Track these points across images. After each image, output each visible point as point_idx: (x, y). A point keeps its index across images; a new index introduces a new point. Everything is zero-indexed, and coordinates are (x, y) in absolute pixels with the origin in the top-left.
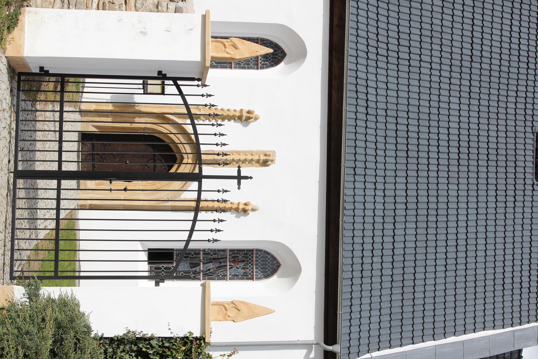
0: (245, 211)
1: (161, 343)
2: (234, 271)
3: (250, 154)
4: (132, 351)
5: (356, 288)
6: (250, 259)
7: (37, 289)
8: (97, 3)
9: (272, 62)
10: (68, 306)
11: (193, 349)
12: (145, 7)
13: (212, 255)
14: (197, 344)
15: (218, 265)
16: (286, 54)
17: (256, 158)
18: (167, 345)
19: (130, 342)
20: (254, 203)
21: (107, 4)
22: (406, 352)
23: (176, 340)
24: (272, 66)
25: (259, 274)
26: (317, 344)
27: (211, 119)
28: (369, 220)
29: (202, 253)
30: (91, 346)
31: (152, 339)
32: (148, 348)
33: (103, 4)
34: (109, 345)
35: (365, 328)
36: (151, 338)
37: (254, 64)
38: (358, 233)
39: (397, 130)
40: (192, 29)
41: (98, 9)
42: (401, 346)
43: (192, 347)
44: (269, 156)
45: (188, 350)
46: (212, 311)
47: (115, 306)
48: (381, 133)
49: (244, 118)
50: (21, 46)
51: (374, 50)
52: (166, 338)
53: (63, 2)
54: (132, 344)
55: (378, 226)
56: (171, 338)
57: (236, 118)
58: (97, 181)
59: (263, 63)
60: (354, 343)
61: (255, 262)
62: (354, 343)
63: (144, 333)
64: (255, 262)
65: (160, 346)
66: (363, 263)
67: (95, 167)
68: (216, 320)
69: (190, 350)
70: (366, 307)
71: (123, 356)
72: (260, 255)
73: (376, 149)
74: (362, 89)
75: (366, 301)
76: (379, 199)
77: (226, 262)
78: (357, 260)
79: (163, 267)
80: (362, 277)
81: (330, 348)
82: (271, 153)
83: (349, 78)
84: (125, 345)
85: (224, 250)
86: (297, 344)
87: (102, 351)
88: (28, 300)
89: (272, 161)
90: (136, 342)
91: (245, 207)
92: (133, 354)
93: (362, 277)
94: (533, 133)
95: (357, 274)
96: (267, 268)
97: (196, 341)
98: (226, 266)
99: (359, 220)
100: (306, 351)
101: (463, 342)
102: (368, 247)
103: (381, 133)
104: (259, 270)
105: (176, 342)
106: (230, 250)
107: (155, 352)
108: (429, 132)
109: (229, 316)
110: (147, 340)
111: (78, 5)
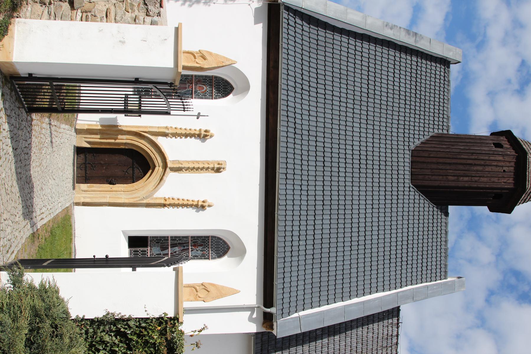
0: (203, 207)
2: (195, 253)
4: (111, 331)
5: (288, 264)
7: (21, 275)
10: (47, 293)
14: (171, 324)
15: (182, 248)
16: (234, 89)
17: (211, 166)
18: (144, 325)
20: (210, 201)
21: (90, 17)
22: (324, 311)
23: (152, 320)
24: (223, 97)
26: (258, 307)
28: (296, 213)
31: (130, 320)
32: (126, 329)
34: (90, 326)
35: (294, 294)
36: (129, 319)
38: (289, 223)
39: (316, 146)
40: (166, 39)
41: (82, 20)
42: (319, 306)
43: (166, 327)
44: (221, 164)
45: (163, 330)
46: (184, 293)
48: (305, 148)
49: (202, 136)
50: (10, 52)
51: (300, 86)
52: (142, 319)
53: (50, 15)
54: (111, 324)
55: (303, 218)
56: (148, 319)
58: (89, 185)
60: (286, 305)
61: (212, 246)
62: (286, 305)
63: (122, 314)
64: (212, 246)
65: (137, 327)
66: (292, 246)
70: (294, 279)
71: (102, 336)
73: (302, 160)
74: (291, 114)
75: (294, 274)
76: (304, 198)
77: (188, 246)
78: (288, 244)
80: (292, 256)
81: (268, 310)
82: (222, 163)
83: (282, 106)
84: (105, 325)
85: (187, 237)
86: (243, 308)
87: (83, 331)
88: (12, 286)
89: (224, 169)
90: (115, 323)
91: (203, 203)
93: (292, 256)
94: (409, 150)
95: (288, 254)
96: (219, 250)
97: (170, 321)
98: (188, 249)
99: (289, 213)
100: (250, 312)
101: (363, 302)
102: (296, 233)
103: (305, 148)
105: (151, 322)
106: (192, 237)
107: (132, 332)
108: (339, 148)
110: (125, 321)
111: (63, 18)
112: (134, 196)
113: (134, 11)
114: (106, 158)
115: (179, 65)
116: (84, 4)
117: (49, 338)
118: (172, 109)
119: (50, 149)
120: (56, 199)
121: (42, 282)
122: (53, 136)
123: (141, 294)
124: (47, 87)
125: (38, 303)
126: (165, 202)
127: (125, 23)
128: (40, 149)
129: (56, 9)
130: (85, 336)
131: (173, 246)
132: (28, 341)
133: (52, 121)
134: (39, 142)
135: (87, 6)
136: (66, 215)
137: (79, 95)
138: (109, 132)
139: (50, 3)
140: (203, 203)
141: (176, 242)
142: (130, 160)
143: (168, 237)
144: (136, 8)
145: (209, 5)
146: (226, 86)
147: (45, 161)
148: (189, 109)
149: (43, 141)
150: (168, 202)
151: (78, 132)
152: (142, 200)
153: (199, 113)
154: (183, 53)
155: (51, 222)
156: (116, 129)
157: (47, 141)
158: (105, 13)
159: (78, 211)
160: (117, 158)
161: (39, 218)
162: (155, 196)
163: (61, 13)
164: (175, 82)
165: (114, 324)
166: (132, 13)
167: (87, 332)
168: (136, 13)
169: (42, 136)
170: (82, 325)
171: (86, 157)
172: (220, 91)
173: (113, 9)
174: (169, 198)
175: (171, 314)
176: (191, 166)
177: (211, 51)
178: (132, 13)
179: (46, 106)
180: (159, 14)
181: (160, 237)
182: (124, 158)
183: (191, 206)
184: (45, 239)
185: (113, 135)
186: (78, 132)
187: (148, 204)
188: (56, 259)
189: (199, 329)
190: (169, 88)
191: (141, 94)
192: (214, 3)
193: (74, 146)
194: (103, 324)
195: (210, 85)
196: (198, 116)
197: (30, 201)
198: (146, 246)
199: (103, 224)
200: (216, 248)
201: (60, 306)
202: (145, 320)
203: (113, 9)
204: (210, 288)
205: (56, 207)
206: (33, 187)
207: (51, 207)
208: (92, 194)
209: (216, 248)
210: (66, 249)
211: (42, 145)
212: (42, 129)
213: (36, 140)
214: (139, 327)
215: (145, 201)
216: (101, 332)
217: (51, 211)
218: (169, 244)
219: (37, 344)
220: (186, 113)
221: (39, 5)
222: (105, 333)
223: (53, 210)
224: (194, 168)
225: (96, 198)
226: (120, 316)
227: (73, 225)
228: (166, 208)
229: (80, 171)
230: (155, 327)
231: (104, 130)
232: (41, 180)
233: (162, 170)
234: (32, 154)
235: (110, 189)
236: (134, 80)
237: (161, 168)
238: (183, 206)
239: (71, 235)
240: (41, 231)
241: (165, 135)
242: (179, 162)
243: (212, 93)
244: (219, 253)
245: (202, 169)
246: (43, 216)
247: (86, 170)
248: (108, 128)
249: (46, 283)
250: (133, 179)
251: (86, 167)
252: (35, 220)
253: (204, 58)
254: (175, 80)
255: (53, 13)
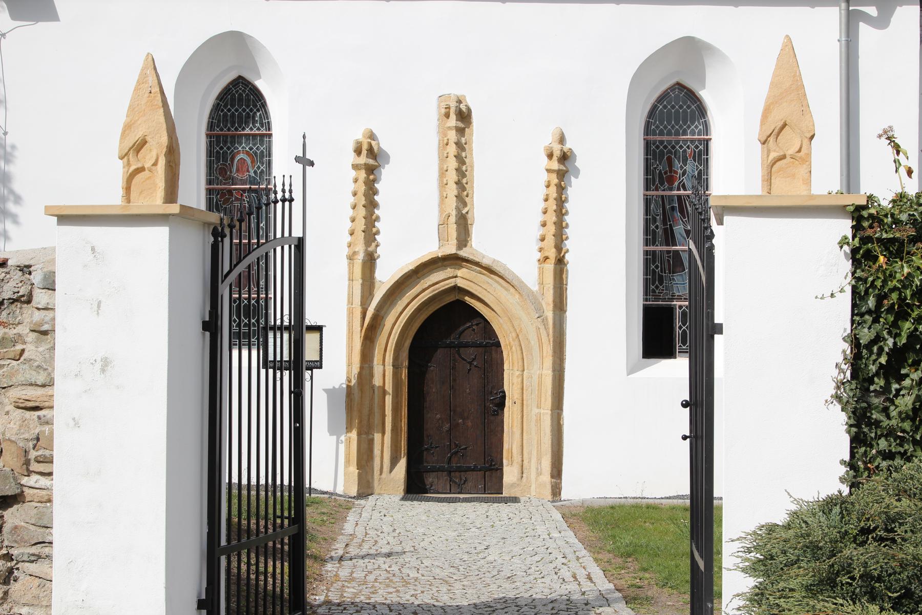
0: (565, 158)
1: (867, 317)
3: (444, 149)
4: (886, 389)
6: (665, 147)
8: (38, 477)
9: (255, 106)
10: (773, 554)
11: (885, 236)
12: (45, 362)
13: (657, 227)
14: (871, 227)
17: (452, 136)
18: (871, 302)
19: (863, 396)
20: (548, 139)
21: (40, 453)
23: (858, 279)
24: (264, 105)
25: (696, 127)
27: (374, 230)
29: (652, 248)
30: (879, 497)
31: (857, 340)
32: (881, 350)
33: (39, 462)
34: (871, 447)
36: (854, 341)
37: (262, 144)
40: (93, 249)
41: (50, 474)
43: (880, 240)
44: (448, 108)
45: (887, 249)
46: (787, 190)
47: (788, 450)
49: (371, 162)
52: (854, 306)
53: (39, 557)
54: (868, 390)
57: (372, 177)
59: (258, 125)
63: (840, 359)
65: (876, 321)
67: (475, 466)
68: (808, 182)
69: (886, 244)
71: (900, 413)
72: (657, 127)
77: (671, 198)
79: (680, 328)
82: (443, 105)
84: (870, 407)
85: (647, 202)
87: (884, 464)
90: (864, 380)
91: (555, 158)
92: (895, 386)
96: (685, 112)
97: (864, 229)
98: (679, 197)
100: (861, 25)
104: (689, 127)
105: (865, 281)
106: (647, 188)
107: (890, 333)
109: (799, 151)
111: (45, 523)
112: (534, 342)
113: (20, 335)
114: (434, 417)
115: (161, 211)
116: (8, 469)
117: (894, 550)
118: (286, 234)
119: (407, 558)
120: (539, 542)
121: (744, 570)
122: (372, 552)
123: (786, 303)
124: (234, 564)
125: (798, 578)
126: (552, 260)
127: (52, 358)
128: (406, 583)
129: (22, 542)
130: (898, 461)
131: (670, 238)
132: (902, 605)
133: (333, 554)
134: (388, 586)
135: (10, 460)
136: (584, 519)
137: (270, 489)
138: (366, 411)
139: (8, 557)
140: (555, 158)
141: (660, 231)
142: (440, 354)
143: (646, 253)
144: (12, 332)
145: (13, 147)
146: (233, 99)
147: (438, 571)
148: (287, 188)
149: (384, 575)
150: (552, 253)
151: (365, 490)
152: (545, 322)
153: (298, 159)
154: (129, 201)
155: (600, 556)
156: (356, 392)
157: (386, 566)
158: (28, 414)
159: (571, 491)
160: (434, 389)
161: (587, 586)
162: (535, 288)
163: (32, 528)
164: (209, 224)
165: (868, 382)
166: (25, 343)
167: (888, 455)
168: (23, 330)
169: (371, 578)
170: (867, 468)
171: (433, 470)
172: (248, 116)
173: (15, 394)
174: (541, 250)
175: (845, 227)
176: (452, 190)
177: (122, 126)
178: (25, 343)
179: (286, 570)
180: (26, 269)
181: (646, 273)
182: (434, 371)
183: (561, 189)
184: (645, 570)
185: (372, 399)
186: (365, 490)
187: (555, 306)
188: (692, 538)
189: (890, 151)
190: (227, 240)
191: (251, 324)
192: (5, 133)
193: (403, 499)
194: (865, 410)
195: (233, 143)
196: (305, 162)
197: (539, 607)
198: (670, 310)
199: (602, 423)
200: (677, 123)
201: (809, 520)
202: (857, 297)
203: (15, 394)
204: (775, 121)
205: (561, 543)
206: (505, 601)
207: (560, 557)
208: (530, 453)
209: (677, 123)
210: (673, 519)
211: (395, 579)
212: (353, 580)
213: (381, 592)
214: (876, 314)
215: (549, 314)
216: (889, 418)
217: (571, 556)
218: (665, 248)
219: (911, 583)
220: (297, 195)
221: (14, 588)
222: (892, 408)
223: (568, 551)
224: (458, 183)
225: (539, 443)
226: (844, 367)
227: (611, 502)
228: (568, 257)
229: (470, 484)
230: (878, 270)
231: (360, 422)
232: (488, 581)
233: (464, 270)
234: (417, 603)
235: (517, 407)
236: (208, 334)
237: (460, 273)
238: (561, 212)
239: (637, 507)
240: (623, 582)
241: (370, 261)
242: (443, 224)
243: (254, 136)
244: (693, 112)
245: (461, 160)
246: (581, 574)
247: (468, 469)
248: (355, 414)
249: (747, 560)
250: (489, 346)
251: (459, 470)
252: (590, 596)
253: (140, 146)
254: (206, 224)
255: (35, 550)
